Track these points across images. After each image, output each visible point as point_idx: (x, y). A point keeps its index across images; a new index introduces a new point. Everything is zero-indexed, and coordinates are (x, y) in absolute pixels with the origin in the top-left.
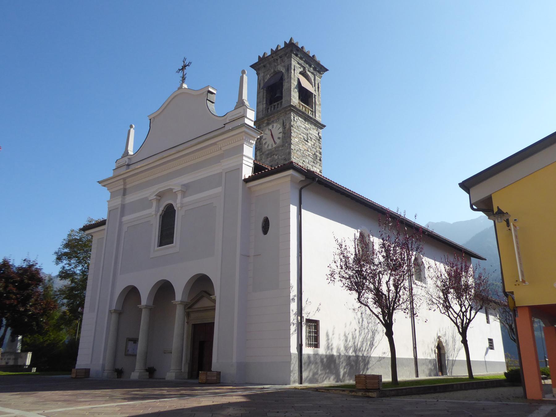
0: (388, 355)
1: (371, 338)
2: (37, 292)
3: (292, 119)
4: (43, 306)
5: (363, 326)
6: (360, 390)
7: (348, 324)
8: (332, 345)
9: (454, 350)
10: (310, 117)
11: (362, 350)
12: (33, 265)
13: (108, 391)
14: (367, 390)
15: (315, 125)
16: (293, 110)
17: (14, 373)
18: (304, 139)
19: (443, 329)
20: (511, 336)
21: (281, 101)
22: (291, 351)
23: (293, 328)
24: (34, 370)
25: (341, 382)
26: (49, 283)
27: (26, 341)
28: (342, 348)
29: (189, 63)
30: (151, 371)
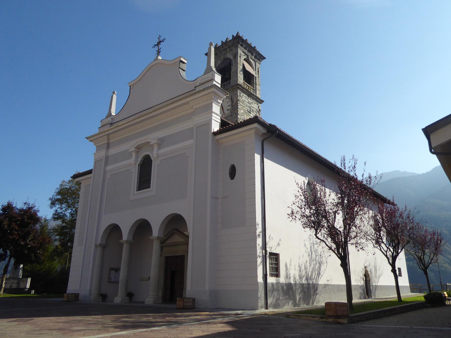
0: (331, 283)
1: (318, 268)
2: (35, 229)
3: (238, 95)
4: (40, 241)
5: (312, 258)
6: (331, 317)
7: (301, 257)
8: (290, 275)
9: (376, 277)
10: (252, 94)
11: (312, 278)
12: (32, 208)
13: (98, 318)
14: (338, 317)
15: (256, 100)
16: (239, 88)
17: (16, 295)
18: (248, 111)
19: (368, 260)
20: (419, 265)
21: (230, 81)
22: (258, 280)
23: (259, 260)
24: (33, 292)
25: (297, 306)
26: (45, 223)
27: (27, 268)
28: (297, 277)
29: (163, 40)
30: (130, 295)
